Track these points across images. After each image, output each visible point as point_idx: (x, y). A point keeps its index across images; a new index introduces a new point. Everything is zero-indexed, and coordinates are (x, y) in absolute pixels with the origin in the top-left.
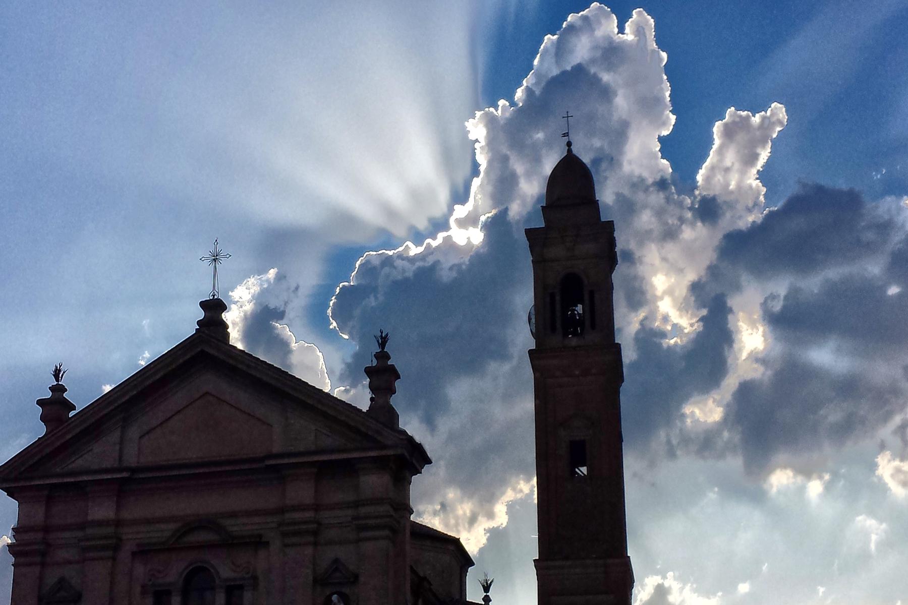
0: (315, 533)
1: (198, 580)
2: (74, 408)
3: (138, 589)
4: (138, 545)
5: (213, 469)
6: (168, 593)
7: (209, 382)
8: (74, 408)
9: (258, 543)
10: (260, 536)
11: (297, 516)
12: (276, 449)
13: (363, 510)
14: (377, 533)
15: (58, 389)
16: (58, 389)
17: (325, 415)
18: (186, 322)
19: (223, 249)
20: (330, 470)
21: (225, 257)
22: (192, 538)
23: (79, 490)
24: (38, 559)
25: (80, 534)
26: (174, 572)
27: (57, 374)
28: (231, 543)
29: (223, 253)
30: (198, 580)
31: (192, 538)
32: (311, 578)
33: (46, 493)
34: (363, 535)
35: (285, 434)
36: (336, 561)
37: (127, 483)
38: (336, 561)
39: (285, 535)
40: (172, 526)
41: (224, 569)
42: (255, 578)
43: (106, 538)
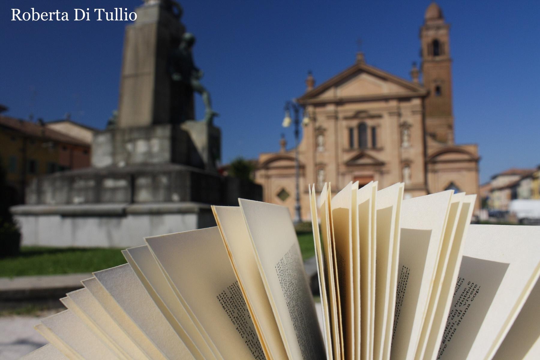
1: (362, 127)
9: (380, 116)
23: (323, 104)
26: (354, 123)
28: (372, 117)
30: (362, 127)
41: (370, 123)
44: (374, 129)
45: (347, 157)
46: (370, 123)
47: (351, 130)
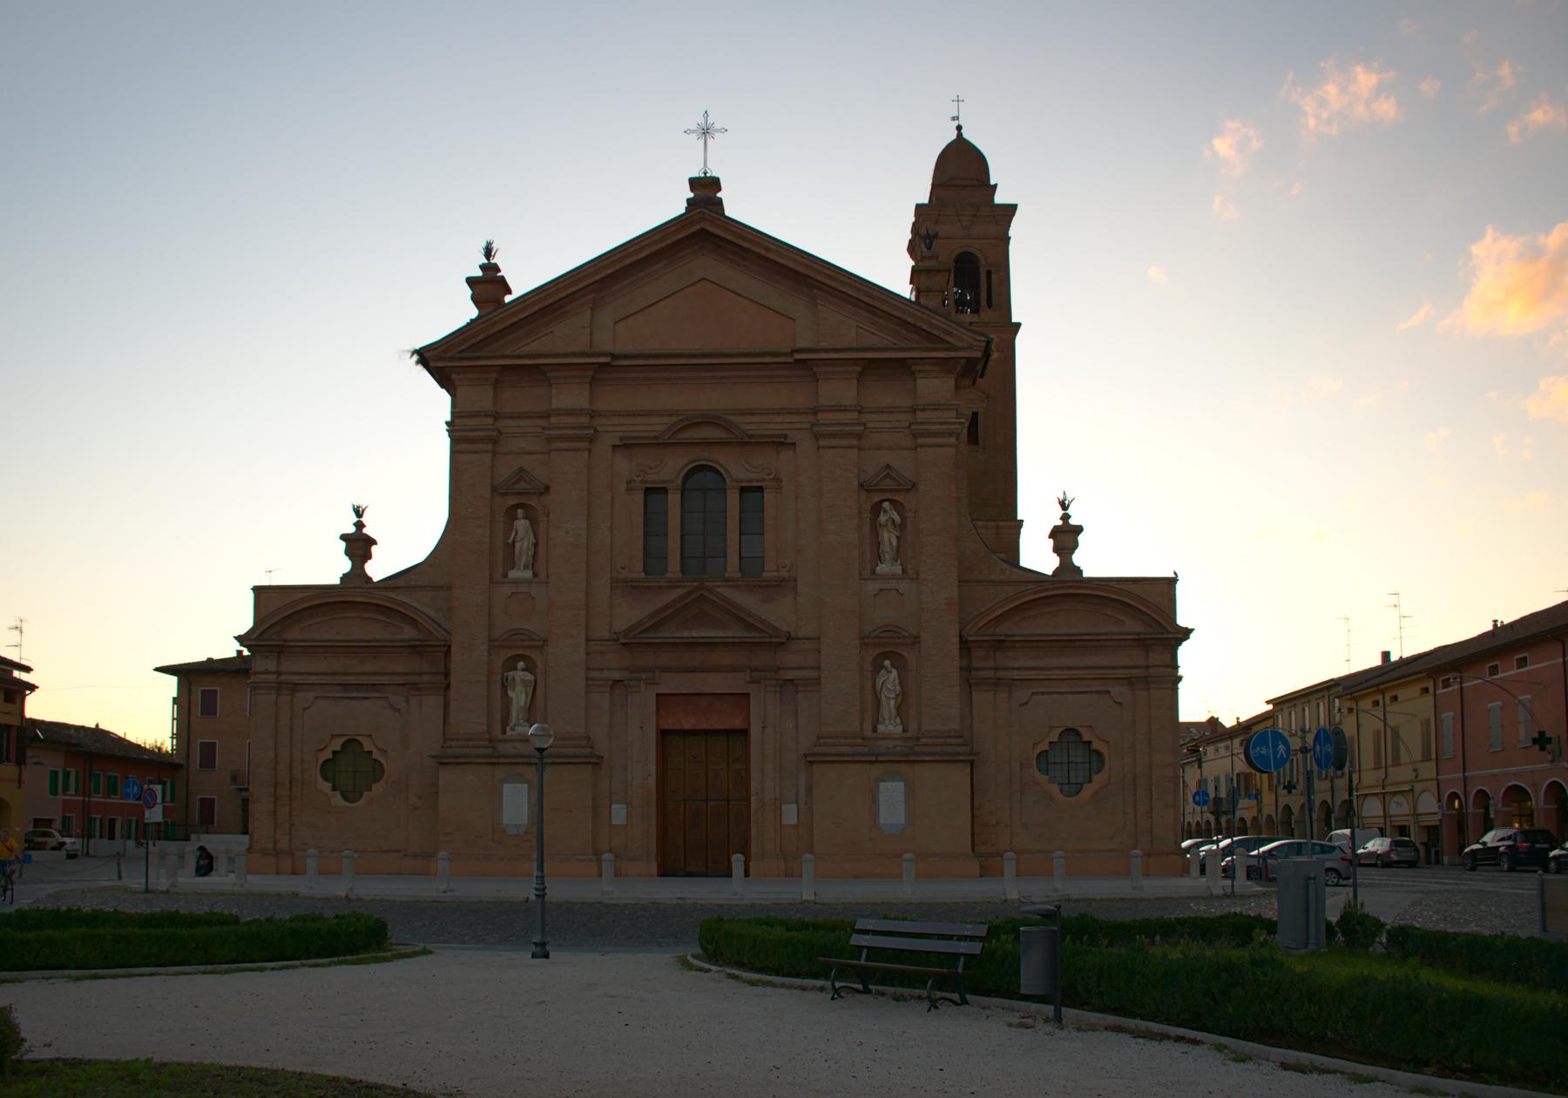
0: (495, 442)
1: (702, 480)
2: (510, 292)
3: (623, 486)
4: (621, 439)
5: (833, 356)
6: (665, 491)
7: (706, 265)
8: (510, 292)
9: (781, 443)
10: (785, 436)
11: (832, 416)
12: (801, 344)
13: (921, 415)
14: (845, 442)
15: (490, 269)
16: (490, 269)
17: (870, 308)
18: (673, 203)
19: (716, 120)
20: (871, 368)
21: (719, 131)
22: (688, 435)
23: (536, 373)
24: (489, 447)
25: (543, 423)
26: (671, 468)
27: (488, 252)
28: (747, 443)
29: (717, 126)
30: (702, 480)
31: (688, 435)
32: (856, 483)
33: (591, 373)
34: (920, 441)
35: (809, 327)
36: (521, 470)
37: (604, 370)
38: (521, 470)
39: (817, 436)
40: (674, 419)
41: (738, 469)
42: (778, 480)
43: (581, 427)
45: (629, 614)
46: (738, 469)
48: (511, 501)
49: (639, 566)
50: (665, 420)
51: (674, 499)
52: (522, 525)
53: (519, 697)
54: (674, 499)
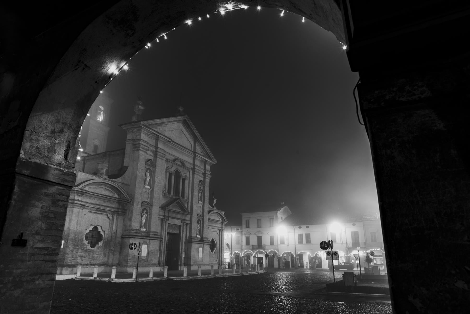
41: (184, 173)
44: (184, 180)
47: (170, 175)
48: (147, 167)
49: (167, 191)
50: (172, 157)
51: (173, 177)
52: (148, 174)
53: (144, 221)
54: (173, 177)
